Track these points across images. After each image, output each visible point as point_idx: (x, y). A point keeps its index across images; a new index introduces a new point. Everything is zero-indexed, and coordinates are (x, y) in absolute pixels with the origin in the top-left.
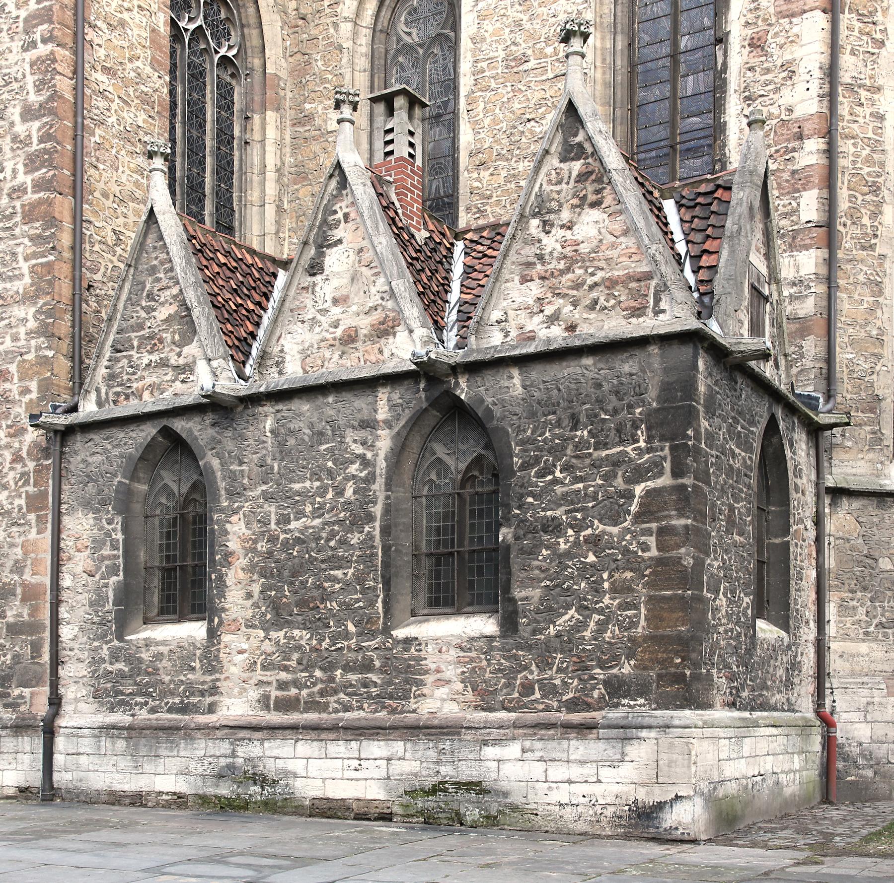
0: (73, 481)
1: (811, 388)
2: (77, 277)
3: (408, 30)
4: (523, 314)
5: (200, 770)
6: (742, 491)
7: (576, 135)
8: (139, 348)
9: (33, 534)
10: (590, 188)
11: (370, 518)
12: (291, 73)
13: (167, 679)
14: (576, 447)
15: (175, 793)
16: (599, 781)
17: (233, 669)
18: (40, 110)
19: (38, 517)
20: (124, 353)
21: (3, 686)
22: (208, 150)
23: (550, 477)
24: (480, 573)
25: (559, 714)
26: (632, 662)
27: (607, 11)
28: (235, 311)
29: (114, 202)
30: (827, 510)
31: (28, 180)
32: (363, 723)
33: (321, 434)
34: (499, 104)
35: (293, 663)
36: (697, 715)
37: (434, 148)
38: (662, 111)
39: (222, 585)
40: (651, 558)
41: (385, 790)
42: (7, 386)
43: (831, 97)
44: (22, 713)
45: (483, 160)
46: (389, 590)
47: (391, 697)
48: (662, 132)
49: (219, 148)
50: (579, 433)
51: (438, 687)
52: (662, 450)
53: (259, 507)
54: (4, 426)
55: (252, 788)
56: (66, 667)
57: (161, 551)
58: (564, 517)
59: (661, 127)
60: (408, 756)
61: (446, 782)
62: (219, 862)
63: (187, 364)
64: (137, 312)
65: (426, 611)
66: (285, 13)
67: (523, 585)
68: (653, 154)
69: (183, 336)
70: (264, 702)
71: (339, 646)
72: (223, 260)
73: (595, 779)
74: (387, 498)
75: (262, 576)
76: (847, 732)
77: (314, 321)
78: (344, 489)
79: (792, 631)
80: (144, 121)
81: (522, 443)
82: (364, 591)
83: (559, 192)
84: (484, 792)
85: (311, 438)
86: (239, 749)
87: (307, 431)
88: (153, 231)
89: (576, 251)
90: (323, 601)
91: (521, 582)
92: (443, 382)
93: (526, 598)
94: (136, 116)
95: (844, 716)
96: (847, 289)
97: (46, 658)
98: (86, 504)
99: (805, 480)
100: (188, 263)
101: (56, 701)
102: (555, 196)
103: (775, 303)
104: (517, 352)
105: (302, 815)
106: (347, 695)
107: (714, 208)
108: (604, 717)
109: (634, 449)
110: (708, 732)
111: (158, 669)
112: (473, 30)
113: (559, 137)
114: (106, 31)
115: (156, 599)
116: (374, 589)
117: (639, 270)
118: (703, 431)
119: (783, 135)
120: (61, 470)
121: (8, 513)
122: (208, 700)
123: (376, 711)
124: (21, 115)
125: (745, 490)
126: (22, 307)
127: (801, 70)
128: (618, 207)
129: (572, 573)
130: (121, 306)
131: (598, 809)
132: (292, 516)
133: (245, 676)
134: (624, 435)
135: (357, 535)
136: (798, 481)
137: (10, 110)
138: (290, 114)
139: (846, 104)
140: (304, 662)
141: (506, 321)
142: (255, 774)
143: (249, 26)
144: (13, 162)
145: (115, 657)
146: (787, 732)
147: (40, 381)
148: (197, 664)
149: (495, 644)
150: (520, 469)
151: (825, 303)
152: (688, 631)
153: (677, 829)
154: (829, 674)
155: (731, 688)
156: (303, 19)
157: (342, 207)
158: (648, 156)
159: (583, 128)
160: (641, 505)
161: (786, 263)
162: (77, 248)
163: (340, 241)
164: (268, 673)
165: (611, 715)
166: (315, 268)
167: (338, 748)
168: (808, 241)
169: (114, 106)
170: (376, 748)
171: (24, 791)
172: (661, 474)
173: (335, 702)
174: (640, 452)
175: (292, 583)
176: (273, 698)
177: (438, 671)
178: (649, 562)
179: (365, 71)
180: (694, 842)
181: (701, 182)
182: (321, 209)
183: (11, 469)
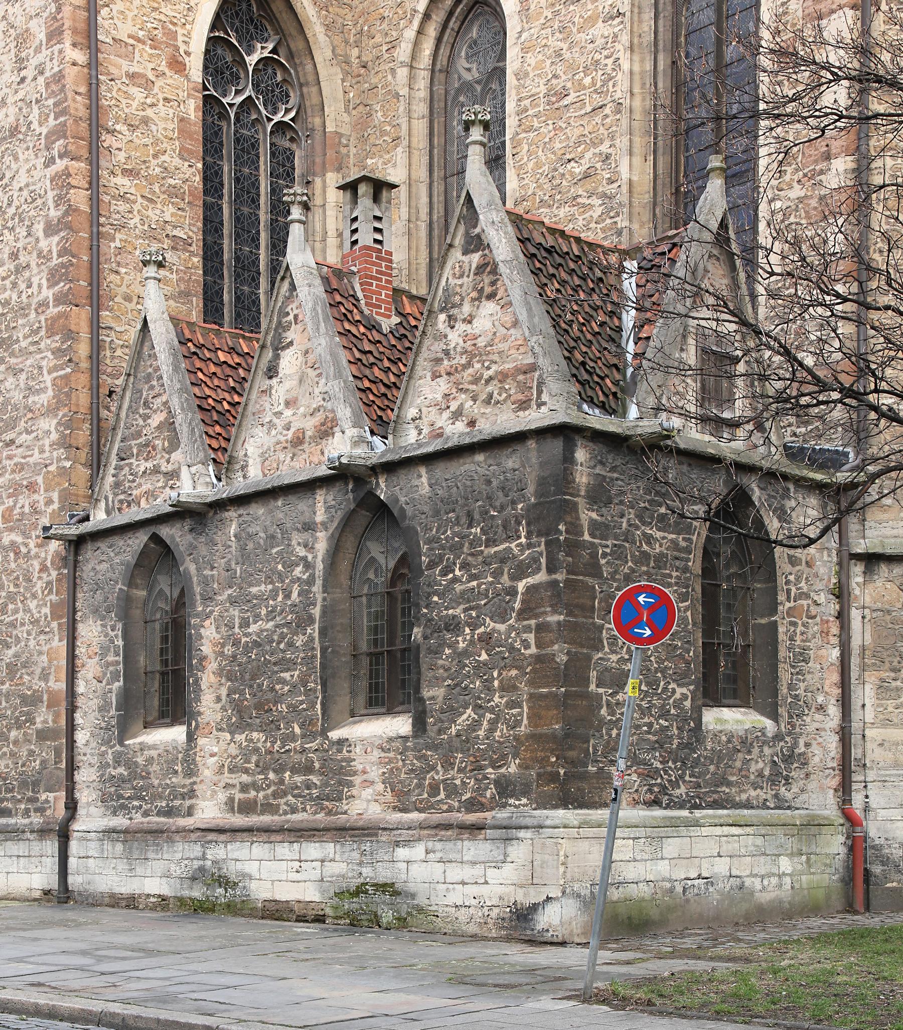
3: (467, 66)
4: (433, 410)
5: (179, 872)
9: (56, 643)
11: (311, 620)
15: (160, 896)
16: (486, 883)
22: (262, 224)
23: (451, 576)
26: (517, 761)
27: (646, 29)
28: (228, 411)
31: (48, 294)
32: (304, 826)
33: (273, 537)
34: (541, 144)
35: (252, 766)
36: (577, 815)
39: (198, 690)
40: (531, 655)
44: (48, 817)
47: (328, 800)
50: (473, 530)
52: (539, 546)
53: (226, 611)
60: (338, 858)
66: (347, 63)
67: (431, 686)
69: (170, 443)
71: (287, 748)
72: (222, 356)
74: (324, 599)
75: (229, 679)
76: (886, 832)
80: (172, 215)
81: (429, 541)
82: (308, 692)
83: (461, 286)
84: (396, 893)
85: (266, 541)
87: (262, 535)
89: (475, 345)
90: (276, 703)
91: (429, 681)
92: (367, 483)
95: (882, 813)
100: (176, 369)
101: (71, 805)
102: (458, 289)
104: (419, 452)
109: (517, 546)
111: (149, 773)
114: (127, 133)
115: (156, 702)
116: (315, 691)
117: (525, 362)
119: (810, 156)
120: (75, 578)
121: (37, 621)
122: (188, 803)
123: (316, 813)
124: (44, 231)
125: (674, 574)
129: (469, 672)
130: (123, 415)
133: (216, 778)
135: (301, 637)
137: (36, 226)
140: (261, 764)
141: (420, 418)
142: (220, 876)
143: (307, 84)
145: (117, 763)
146: (763, 832)
147: (60, 491)
148: (179, 768)
152: (562, 729)
153: (548, 931)
160: (523, 602)
164: (233, 776)
165: (499, 815)
167: (284, 850)
170: (313, 850)
171: (47, 893)
172: (539, 569)
175: (251, 686)
179: (423, 117)
180: (563, 944)
183: (40, 578)
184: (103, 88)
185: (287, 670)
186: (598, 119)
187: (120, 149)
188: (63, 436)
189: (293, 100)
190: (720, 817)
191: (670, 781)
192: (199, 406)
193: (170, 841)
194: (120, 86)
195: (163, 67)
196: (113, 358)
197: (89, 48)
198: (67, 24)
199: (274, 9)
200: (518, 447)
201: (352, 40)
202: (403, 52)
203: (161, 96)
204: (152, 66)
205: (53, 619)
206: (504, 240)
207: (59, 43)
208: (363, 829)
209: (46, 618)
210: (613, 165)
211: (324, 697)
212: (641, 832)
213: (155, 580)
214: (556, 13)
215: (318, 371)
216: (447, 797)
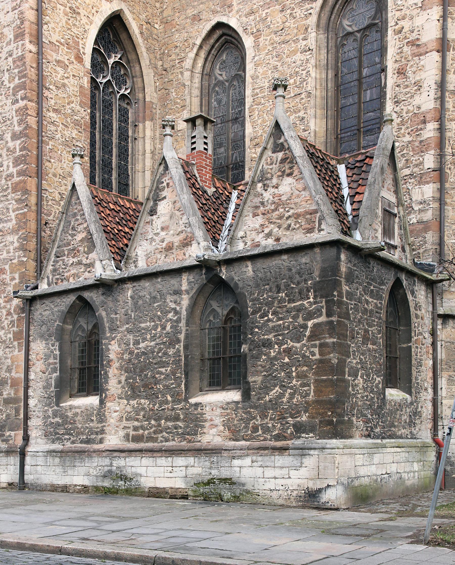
0: (35, 324)
1: (430, 260)
2: (39, 219)
3: (220, 73)
4: (254, 233)
5: (95, 473)
6: (374, 321)
7: (280, 139)
8: (68, 255)
9: (16, 352)
10: (287, 166)
11: (179, 341)
12: (159, 99)
13: (80, 426)
14: (279, 302)
15: (83, 485)
16: (290, 478)
17: (112, 421)
18: (20, 134)
19: (19, 343)
20: (61, 258)
21: (1, 431)
22: (114, 145)
23: (266, 318)
24: (235, 369)
25: (271, 442)
26: (307, 414)
27: (323, 58)
28: (117, 234)
29: (59, 178)
30: (439, 327)
31: (15, 170)
32: (174, 448)
33: (155, 298)
34: (265, 111)
35: (141, 417)
37: (234, 136)
38: (353, 111)
40: (316, 360)
41: (185, 483)
42: (4, 276)
43: (442, 99)
44: (10, 444)
45: (257, 142)
46: (187, 378)
47: (188, 434)
48: (354, 122)
49: (120, 143)
50: (280, 295)
51: (211, 429)
52: (321, 303)
53: (125, 336)
54: (3, 297)
55: (120, 482)
56: (32, 420)
57: (79, 359)
58: (273, 339)
59: (353, 119)
60: (196, 465)
61: (214, 478)
62: (83, 519)
63: (91, 263)
64: (67, 237)
65: (207, 389)
67: (253, 375)
68: (349, 134)
70: (127, 437)
71: (163, 408)
72: (112, 206)
73: (287, 477)
74: (187, 330)
75: (126, 372)
77: (152, 240)
78: (166, 326)
79: (414, 394)
80: (76, 135)
81: (253, 300)
83: (271, 169)
84: (233, 483)
85: (150, 300)
86: (114, 462)
87: (148, 296)
88: (75, 195)
89: (280, 199)
90: (156, 384)
92: (214, 270)
93: (255, 382)
94: (72, 132)
96: (451, 204)
97: (22, 416)
98: (42, 336)
99: (423, 311)
100: (92, 211)
101: (26, 438)
102: (270, 171)
103: (402, 216)
104: (249, 254)
105: (144, 497)
106: (167, 433)
107: (363, 169)
108: (293, 444)
109: (308, 303)
110: (347, 451)
111: (76, 421)
112: (252, 72)
113: (272, 140)
114: (55, 90)
115: (76, 384)
116: (180, 378)
118: (344, 292)
119: (415, 121)
120: (29, 319)
121: (5, 341)
122: (100, 436)
123: (181, 442)
125: (376, 320)
126: (12, 236)
127: (425, 85)
128: (301, 176)
129: (277, 368)
130: (59, 234)
131: (289, 492)
132: (141, 341)
133: (118, 424)
134: (303, 295)
135: (172, 350)
136: (418, 312)
137: (6, 135)
138: (159, 122)
139: (451, 102)
140: (146, 416)
141: (246, 237)
142: (121, 475)
143: (136, 77)
144: (7, 162)
145: (55, 415)
146: (408, 450)
147: (20, 273)
148: (94, 418)
149: (239, 405)
150: (252, 314)
151: (438, 213)
152: (335, 397)
153: (328, 502)
154: (442, 417)
155: (367, 427)
156: (165, 70)
157: (166, 180)
158: (346, 135)
159: (283, 134)
160: (311, 332)
161: (417, 192)
162: (39, 204)
163: (165, 198)
164: (129, 422)
165: (296, 443)
166: (153, 212)
167: (162, 461)
168: (429, 179)
169: (59, 129)
170: (180, 461)
171: (10, 484)
172: (321, 315)
173: (161, 437)
174: (311, 304)
175: (140, 376)
176: (131, 435)
177: (211, 420)
178: (315, 362)
179: (197, 97)
180: (337, 509)
181: (359, 154)
182: (156, 181)
183: (6, 319)
184: (44, 66)
185: (163, 367)
186: (298, 100)
187: (52, 98)
188: (22, 245)
189: (129, 84)
190: (392, 443)
191: (374, 425)
192: (104, 230)
193: (90, 456)
194: (52, 66)
195: (73, 59)
196: (47, 205)
197: (38, 44)
198: (27, 31)
199: (121, 38)
200: (309, 252)
201: (158, 57)
202: (188, 63)
203: (71, 74)
204: (67, 57)
205: (14, 340)
206: (298, 146)
207: (22, 40)
208: (212, 450)
209: (10, 339)
210: (306, 123)
211: (186, 381)
212: (365, 451)
213: (77, 320)
214: (274, 48)
215: (182, 212)
216: (263, 433)
